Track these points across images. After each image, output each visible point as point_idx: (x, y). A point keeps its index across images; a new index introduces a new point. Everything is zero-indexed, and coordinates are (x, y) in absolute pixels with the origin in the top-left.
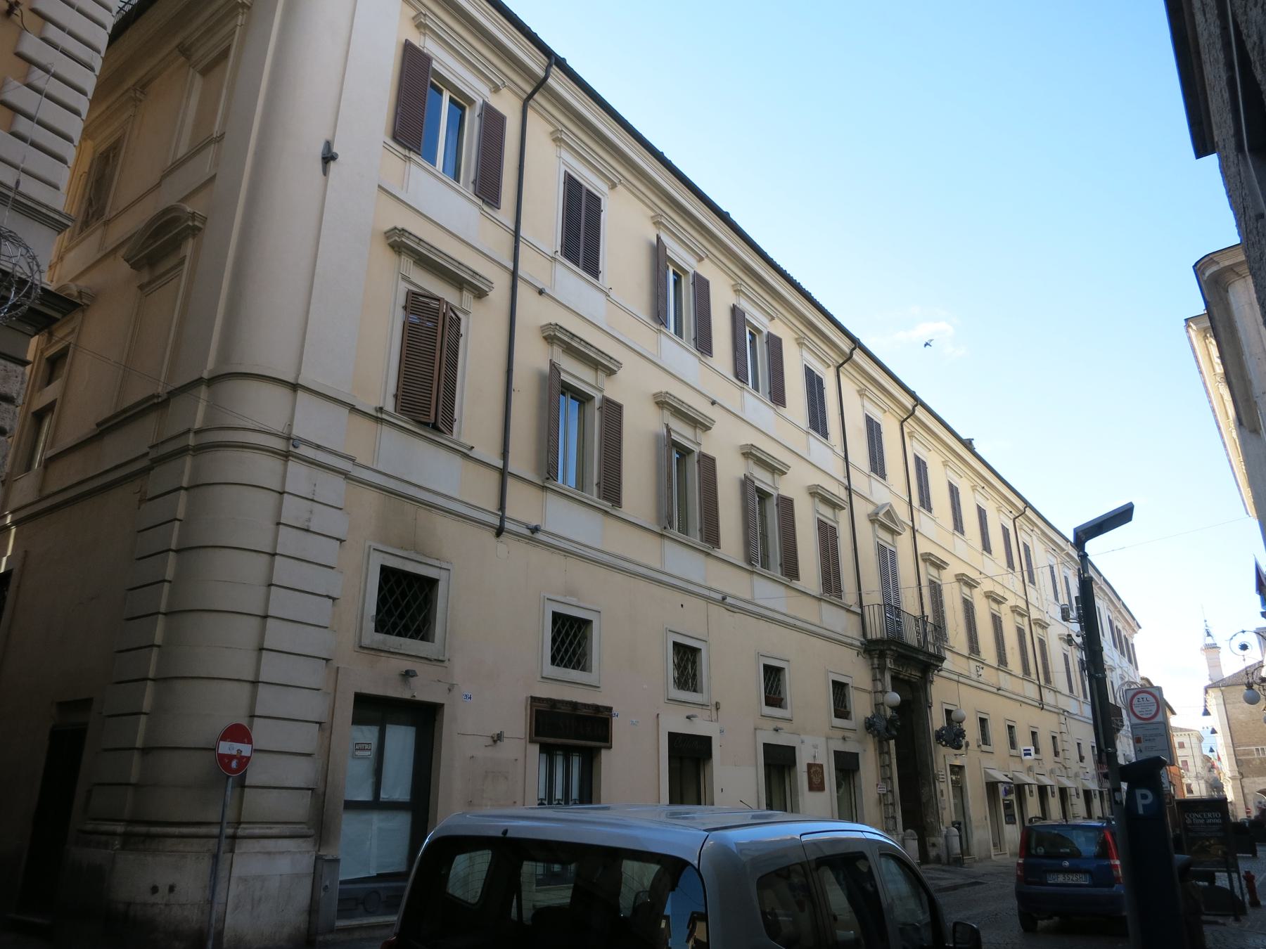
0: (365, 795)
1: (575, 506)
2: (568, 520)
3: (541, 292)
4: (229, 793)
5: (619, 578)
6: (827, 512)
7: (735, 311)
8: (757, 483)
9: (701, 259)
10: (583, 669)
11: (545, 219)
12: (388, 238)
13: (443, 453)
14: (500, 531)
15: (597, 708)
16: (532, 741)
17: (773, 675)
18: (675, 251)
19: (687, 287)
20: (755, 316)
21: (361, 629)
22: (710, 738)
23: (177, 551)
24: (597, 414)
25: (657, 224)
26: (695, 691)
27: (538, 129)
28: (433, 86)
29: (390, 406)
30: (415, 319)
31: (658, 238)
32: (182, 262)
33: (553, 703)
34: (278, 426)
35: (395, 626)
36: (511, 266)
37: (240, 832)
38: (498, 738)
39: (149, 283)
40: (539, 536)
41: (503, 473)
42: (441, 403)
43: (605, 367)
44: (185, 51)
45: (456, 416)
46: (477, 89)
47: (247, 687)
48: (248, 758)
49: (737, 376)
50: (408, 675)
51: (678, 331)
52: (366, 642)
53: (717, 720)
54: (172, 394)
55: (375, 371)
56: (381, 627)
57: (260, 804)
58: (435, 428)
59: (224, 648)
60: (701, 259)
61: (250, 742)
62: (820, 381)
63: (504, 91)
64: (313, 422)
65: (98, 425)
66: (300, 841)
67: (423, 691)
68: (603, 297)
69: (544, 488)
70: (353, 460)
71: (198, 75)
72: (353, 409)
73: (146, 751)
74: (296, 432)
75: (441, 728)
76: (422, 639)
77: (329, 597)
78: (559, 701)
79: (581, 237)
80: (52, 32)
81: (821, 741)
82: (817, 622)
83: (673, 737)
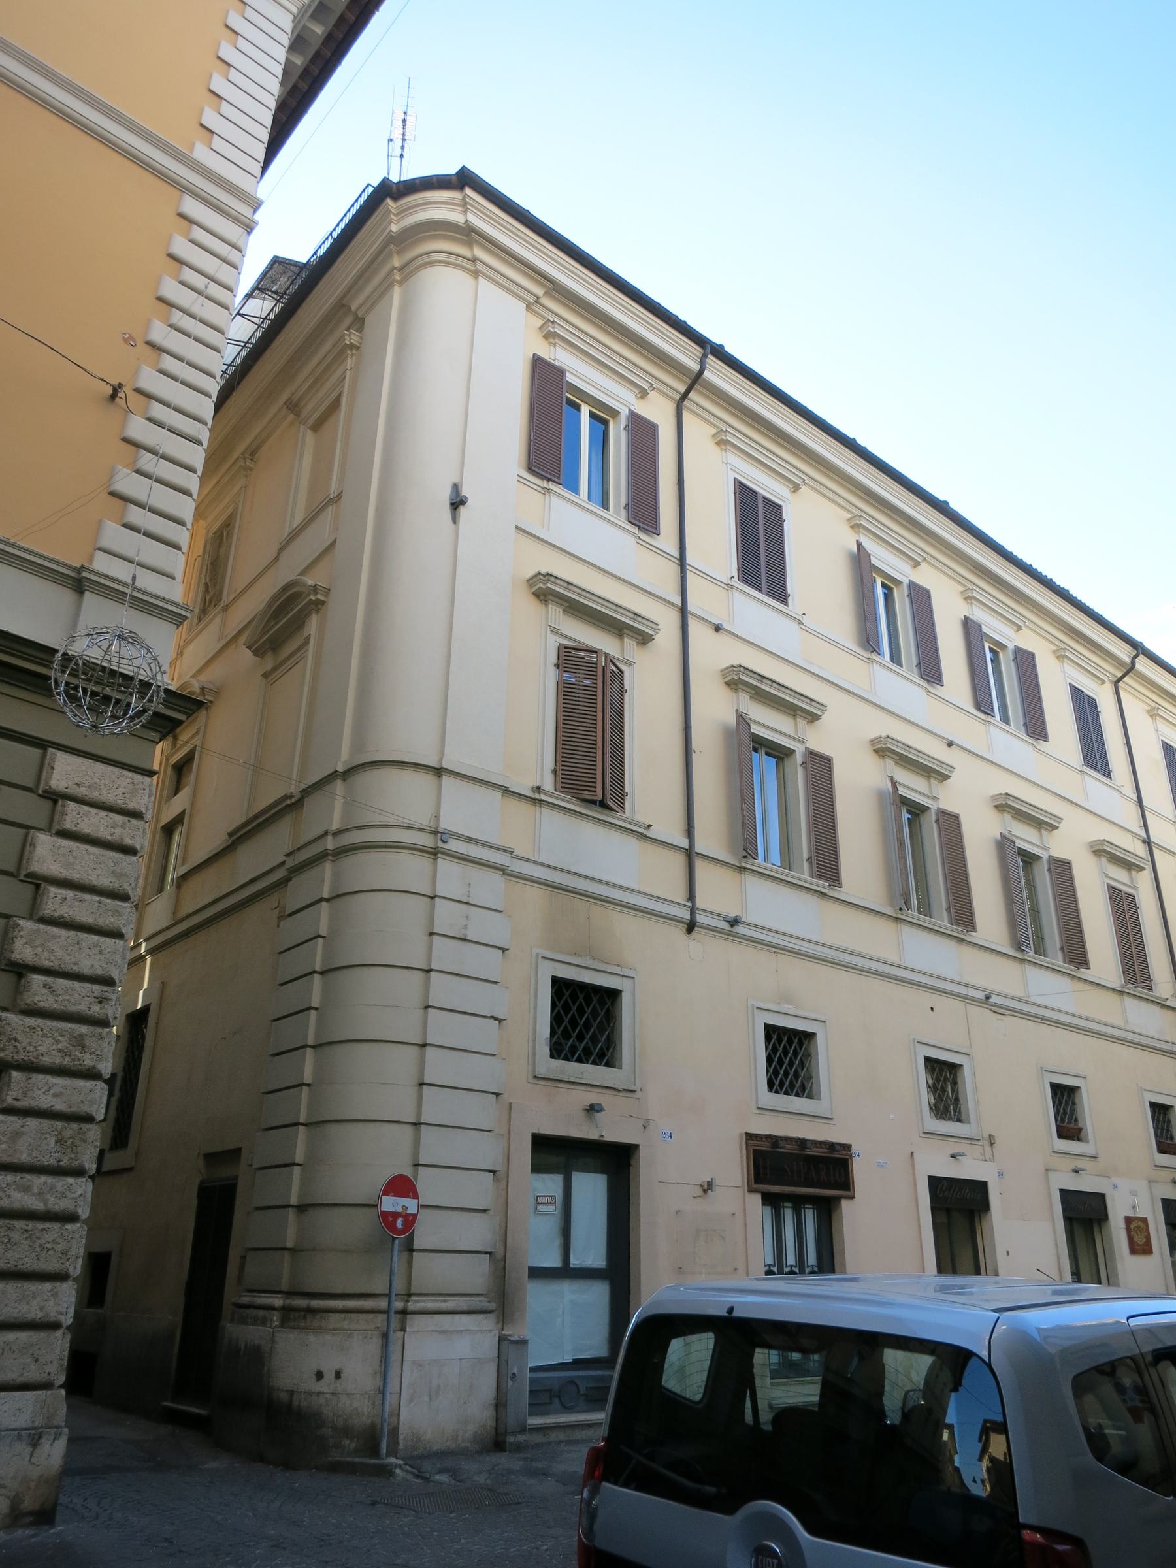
2: (774, 906)
3: (718, 629)
4: (395, 1259)
5: (845, 976)
6: (1119, 875)
7: (970, 628)
8: (1019, 844)
10: (810, 1096)
12: (531, 586)
13: (616, 836)
14: (691, 927)
15: (831, 1146)
16: (751, 1190)
17: (1064, 1097)
18: (881, 557)
20: (994, 627)
21: (534, 1054)
22: (984, 1185)
23: (322, 973)
24: (800, 772)
25: (856, 527)
26: (959, 1121)
27: (697, 432)
28: (570, 403)
29: (548, 784)
30: (569, 678)
31: (859, 545)
32: (307, 641)
33: (775, 1140)
34: (424, 820)
35: (573, 1050)
36: (678, 602)
37: (411, 1306)
38: (707, 1188)
39: (275, 669)
40: (740, 929)
41: (690, 854)
43: (803, 711)
44: (293, 407)
45: (627, 789)
47: (409, 1130)
48: (415, 1216)
49: (978, 708)
51: (896, 658)
52: (541, 1071)
53: (992, 1160)
54: (306, 792)
56: (557, 1051)
57: (431, 1271)
58: (603, 805)
59: (376, 1084)
60: (917, 564)
61: (416, 1196)
62: (1093, 703)
63: (653, 395)
64: (463, 811)
65: (230, 835)
67: (612, 1129)
68: (795, 625)
69: (742, 869)
71: (309, 432)
72: (506, 791)
73: (302, 1208)
74: (444, 825)
76: (607, 1065)
77: (496, 1019)
81: (1142, 1186)
82: (1121, 1024)
83: (937, 1184)
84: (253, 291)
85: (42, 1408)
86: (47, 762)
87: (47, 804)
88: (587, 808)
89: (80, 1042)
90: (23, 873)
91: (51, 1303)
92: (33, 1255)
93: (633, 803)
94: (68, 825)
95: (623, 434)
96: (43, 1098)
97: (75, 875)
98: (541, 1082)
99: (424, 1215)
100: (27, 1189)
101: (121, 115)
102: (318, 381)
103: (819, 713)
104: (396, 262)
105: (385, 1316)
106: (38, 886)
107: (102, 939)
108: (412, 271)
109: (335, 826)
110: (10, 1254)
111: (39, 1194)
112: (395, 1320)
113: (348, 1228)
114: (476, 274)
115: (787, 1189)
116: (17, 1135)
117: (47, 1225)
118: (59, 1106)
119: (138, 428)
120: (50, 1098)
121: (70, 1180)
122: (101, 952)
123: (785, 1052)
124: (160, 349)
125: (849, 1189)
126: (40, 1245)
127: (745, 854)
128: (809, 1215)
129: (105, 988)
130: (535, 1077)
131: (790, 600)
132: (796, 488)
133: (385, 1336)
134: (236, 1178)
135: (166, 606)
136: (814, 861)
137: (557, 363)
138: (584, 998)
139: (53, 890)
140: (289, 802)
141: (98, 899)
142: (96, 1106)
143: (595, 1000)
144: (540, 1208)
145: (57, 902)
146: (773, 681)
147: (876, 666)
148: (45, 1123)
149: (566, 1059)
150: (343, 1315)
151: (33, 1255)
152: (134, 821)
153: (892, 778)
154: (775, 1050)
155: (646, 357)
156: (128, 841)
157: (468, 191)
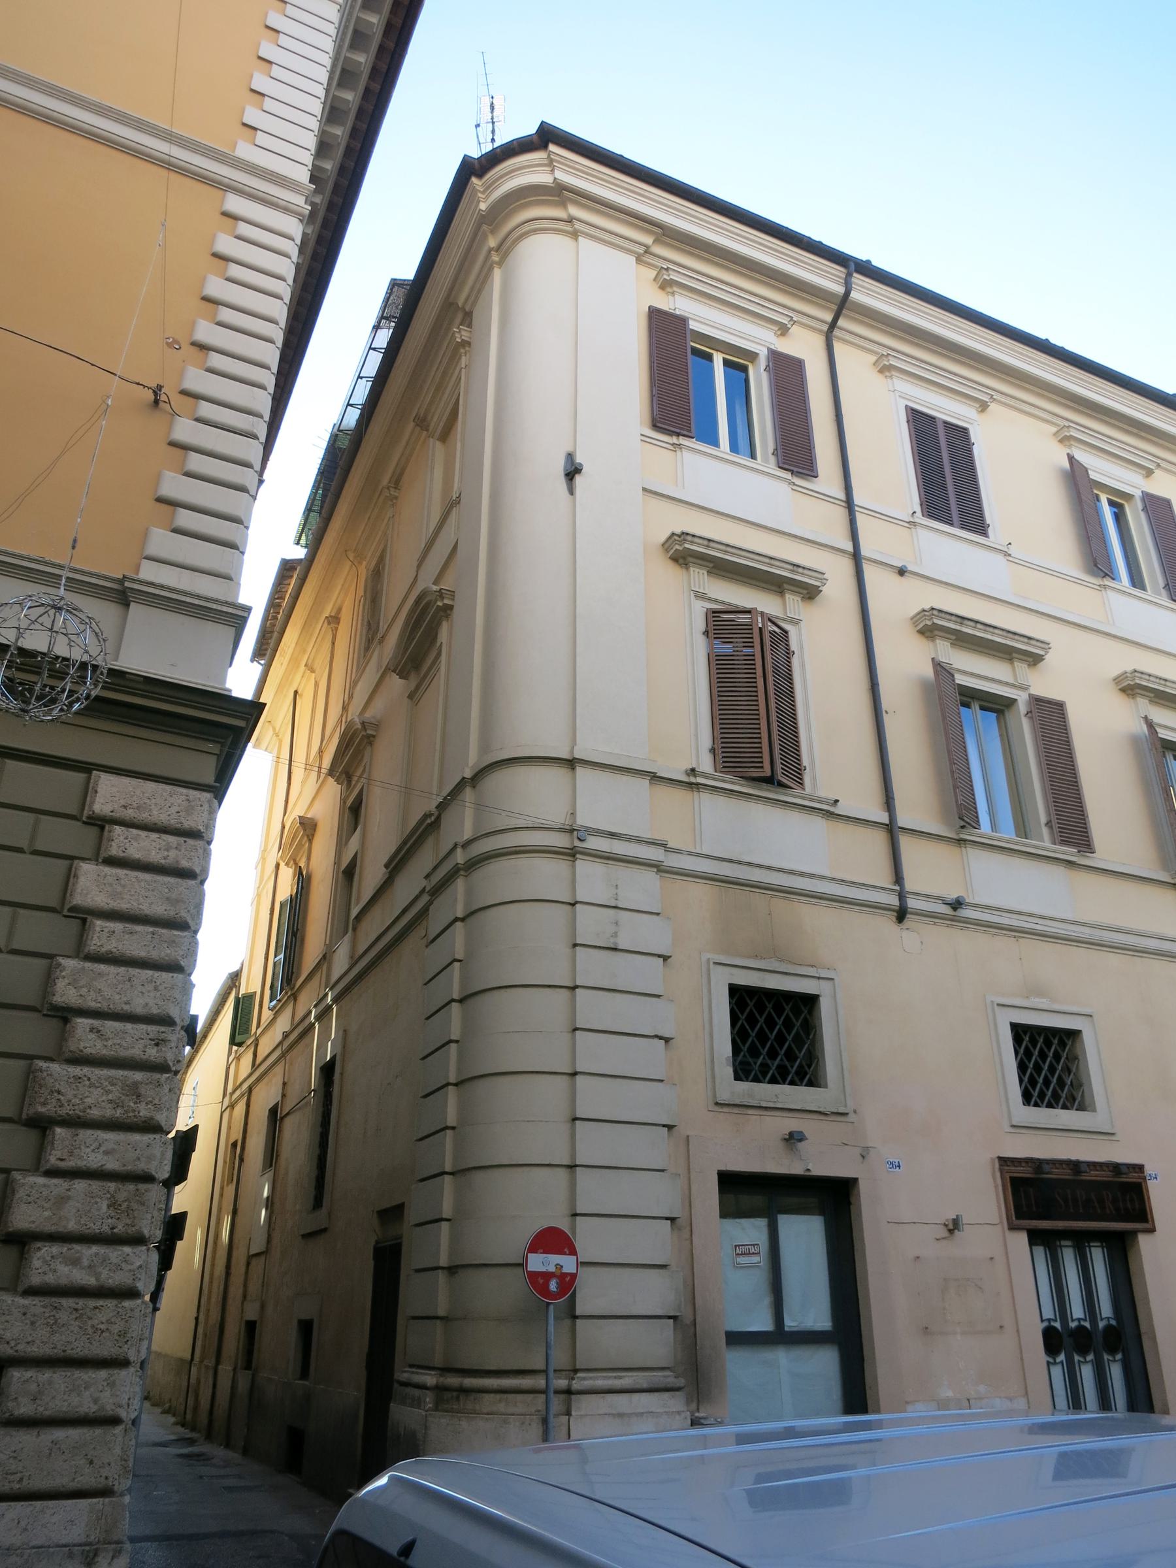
0: (762, 1322)
1: (1018, 861)
2: (1004, 882)
3: (902, 572)
4: (551, 1328)
5: (1114, 960)
9: (1149, 473)
10: (1082, 1108)
11: (888, 472)
12: (667, 551)
13: (795, 817)
14: (901, 914)
15: (1116, 1168)
16: (1012, 1228)
18: (1101, 469)
19: (1137, 518)
21: (713, 1077)
23: (461, 1001)
24: (1026, 725)
25: (1065, 440)
27: (854, 363)
28: (696, 352)
29: (706, 764)
30: (727, 649)
31: (1071, 458)
32: (439, 654)
34: (559, 817)
35: (764, 1069)
36: (849, 547)
37: (576, 1385)
38: (954, 1226)
39: (417, 688)
40: (966, 913)
41: (892, 830)
42: (776, 747)
43: (1028, 655)
44: (422, 423)
45: (805, 761)
46: (757, 338)
47: (563, 1174)
48: (573, 1276)
50: (793, 1139)
51: (1137, 580)
52: (724, 1096)
54: (442, 806)
55: (678, 719)
56: (742, 1072)
57: (601, 1342)
58: (770, 780)
59: (523, 1123)
60: (1149, 473)
61: (573, 1252)
63: (795, 330)
64: (602, 804)
65: (386, 866)
66: (666, 1396)
67: (822, 1160)
69: (960, 842)
70: (664, 845)
71: (438, 443)
72: (654, 778)
73: (452, 1270)
74: (581, 821)
75: (860, 1215)
76: (811, 1084)
77: (661, 1038)
78: (1048, 1162)
79: (947, 479)
80: (206, 410)
84: (379, 322)
85: (99, 1519)
86: (91, 785)
87: (94, 831)
88: (754, 788)
89: (134, 1091)
90: (67, 907)
91: (107, 1393)
92: (84, 1338)
93: (814, 778)
94: (115, 850)
95: (765, 377)
96: (92, 1156)
97: (123, 905)
98: (725, 1110)
99: (585, 1275)
100: (75, 1262)
101: (155, 127)
102: (440, 388)
103: (1041, 652)
104: (492, 242)
105: (543, 1396)
106: (84, 921)
107: (157, 974)
108: (509, 248)
109: (467, 834)
110: (56, 1337)
111: (90, 1267)
112: (556, 1403)
113: (499, 1293)
114: (575, 235)
115: (1060, 1225)
116: (62, 1200)
117: (101, 1302)
118: (112, 1165)
119: (185, 430)
120: (99, 1156)
121: (127, 1249)
122: (156, 989)
123: (1042, 1055)
124: (203, 348)
125: (1146, 1221)
126: (93, 1326)
127: (963, 823)
128: (1098, 1257)
129: (163, 1029)
130: (717, 1104)
131: (990, 531)
132: (983, 407)
133: (545, 1421)
134: (401, 1237)
135: (219, 608)
136: (1055, 826)
137: (678, 312)
138: (774, 1008)
139: (99, 923)
140: (429, 821)
141: (151, 929)
142: (155, 1163)
143: (769, 1006)
144: (741, 1260)
145: (104, 936)
146: (977, 622)
147: (1110, 593)
148: (95, 1185)
149: (756, 1080)
150: (498, 1396)
151: (84, 1338)
152: (191, 842)
153: (1146, 718)
154: (1028, 1053)
155: (780, 290)
156: (184, 864)
157: (552, 147)
